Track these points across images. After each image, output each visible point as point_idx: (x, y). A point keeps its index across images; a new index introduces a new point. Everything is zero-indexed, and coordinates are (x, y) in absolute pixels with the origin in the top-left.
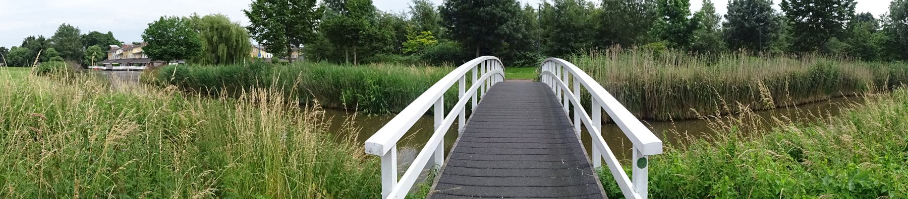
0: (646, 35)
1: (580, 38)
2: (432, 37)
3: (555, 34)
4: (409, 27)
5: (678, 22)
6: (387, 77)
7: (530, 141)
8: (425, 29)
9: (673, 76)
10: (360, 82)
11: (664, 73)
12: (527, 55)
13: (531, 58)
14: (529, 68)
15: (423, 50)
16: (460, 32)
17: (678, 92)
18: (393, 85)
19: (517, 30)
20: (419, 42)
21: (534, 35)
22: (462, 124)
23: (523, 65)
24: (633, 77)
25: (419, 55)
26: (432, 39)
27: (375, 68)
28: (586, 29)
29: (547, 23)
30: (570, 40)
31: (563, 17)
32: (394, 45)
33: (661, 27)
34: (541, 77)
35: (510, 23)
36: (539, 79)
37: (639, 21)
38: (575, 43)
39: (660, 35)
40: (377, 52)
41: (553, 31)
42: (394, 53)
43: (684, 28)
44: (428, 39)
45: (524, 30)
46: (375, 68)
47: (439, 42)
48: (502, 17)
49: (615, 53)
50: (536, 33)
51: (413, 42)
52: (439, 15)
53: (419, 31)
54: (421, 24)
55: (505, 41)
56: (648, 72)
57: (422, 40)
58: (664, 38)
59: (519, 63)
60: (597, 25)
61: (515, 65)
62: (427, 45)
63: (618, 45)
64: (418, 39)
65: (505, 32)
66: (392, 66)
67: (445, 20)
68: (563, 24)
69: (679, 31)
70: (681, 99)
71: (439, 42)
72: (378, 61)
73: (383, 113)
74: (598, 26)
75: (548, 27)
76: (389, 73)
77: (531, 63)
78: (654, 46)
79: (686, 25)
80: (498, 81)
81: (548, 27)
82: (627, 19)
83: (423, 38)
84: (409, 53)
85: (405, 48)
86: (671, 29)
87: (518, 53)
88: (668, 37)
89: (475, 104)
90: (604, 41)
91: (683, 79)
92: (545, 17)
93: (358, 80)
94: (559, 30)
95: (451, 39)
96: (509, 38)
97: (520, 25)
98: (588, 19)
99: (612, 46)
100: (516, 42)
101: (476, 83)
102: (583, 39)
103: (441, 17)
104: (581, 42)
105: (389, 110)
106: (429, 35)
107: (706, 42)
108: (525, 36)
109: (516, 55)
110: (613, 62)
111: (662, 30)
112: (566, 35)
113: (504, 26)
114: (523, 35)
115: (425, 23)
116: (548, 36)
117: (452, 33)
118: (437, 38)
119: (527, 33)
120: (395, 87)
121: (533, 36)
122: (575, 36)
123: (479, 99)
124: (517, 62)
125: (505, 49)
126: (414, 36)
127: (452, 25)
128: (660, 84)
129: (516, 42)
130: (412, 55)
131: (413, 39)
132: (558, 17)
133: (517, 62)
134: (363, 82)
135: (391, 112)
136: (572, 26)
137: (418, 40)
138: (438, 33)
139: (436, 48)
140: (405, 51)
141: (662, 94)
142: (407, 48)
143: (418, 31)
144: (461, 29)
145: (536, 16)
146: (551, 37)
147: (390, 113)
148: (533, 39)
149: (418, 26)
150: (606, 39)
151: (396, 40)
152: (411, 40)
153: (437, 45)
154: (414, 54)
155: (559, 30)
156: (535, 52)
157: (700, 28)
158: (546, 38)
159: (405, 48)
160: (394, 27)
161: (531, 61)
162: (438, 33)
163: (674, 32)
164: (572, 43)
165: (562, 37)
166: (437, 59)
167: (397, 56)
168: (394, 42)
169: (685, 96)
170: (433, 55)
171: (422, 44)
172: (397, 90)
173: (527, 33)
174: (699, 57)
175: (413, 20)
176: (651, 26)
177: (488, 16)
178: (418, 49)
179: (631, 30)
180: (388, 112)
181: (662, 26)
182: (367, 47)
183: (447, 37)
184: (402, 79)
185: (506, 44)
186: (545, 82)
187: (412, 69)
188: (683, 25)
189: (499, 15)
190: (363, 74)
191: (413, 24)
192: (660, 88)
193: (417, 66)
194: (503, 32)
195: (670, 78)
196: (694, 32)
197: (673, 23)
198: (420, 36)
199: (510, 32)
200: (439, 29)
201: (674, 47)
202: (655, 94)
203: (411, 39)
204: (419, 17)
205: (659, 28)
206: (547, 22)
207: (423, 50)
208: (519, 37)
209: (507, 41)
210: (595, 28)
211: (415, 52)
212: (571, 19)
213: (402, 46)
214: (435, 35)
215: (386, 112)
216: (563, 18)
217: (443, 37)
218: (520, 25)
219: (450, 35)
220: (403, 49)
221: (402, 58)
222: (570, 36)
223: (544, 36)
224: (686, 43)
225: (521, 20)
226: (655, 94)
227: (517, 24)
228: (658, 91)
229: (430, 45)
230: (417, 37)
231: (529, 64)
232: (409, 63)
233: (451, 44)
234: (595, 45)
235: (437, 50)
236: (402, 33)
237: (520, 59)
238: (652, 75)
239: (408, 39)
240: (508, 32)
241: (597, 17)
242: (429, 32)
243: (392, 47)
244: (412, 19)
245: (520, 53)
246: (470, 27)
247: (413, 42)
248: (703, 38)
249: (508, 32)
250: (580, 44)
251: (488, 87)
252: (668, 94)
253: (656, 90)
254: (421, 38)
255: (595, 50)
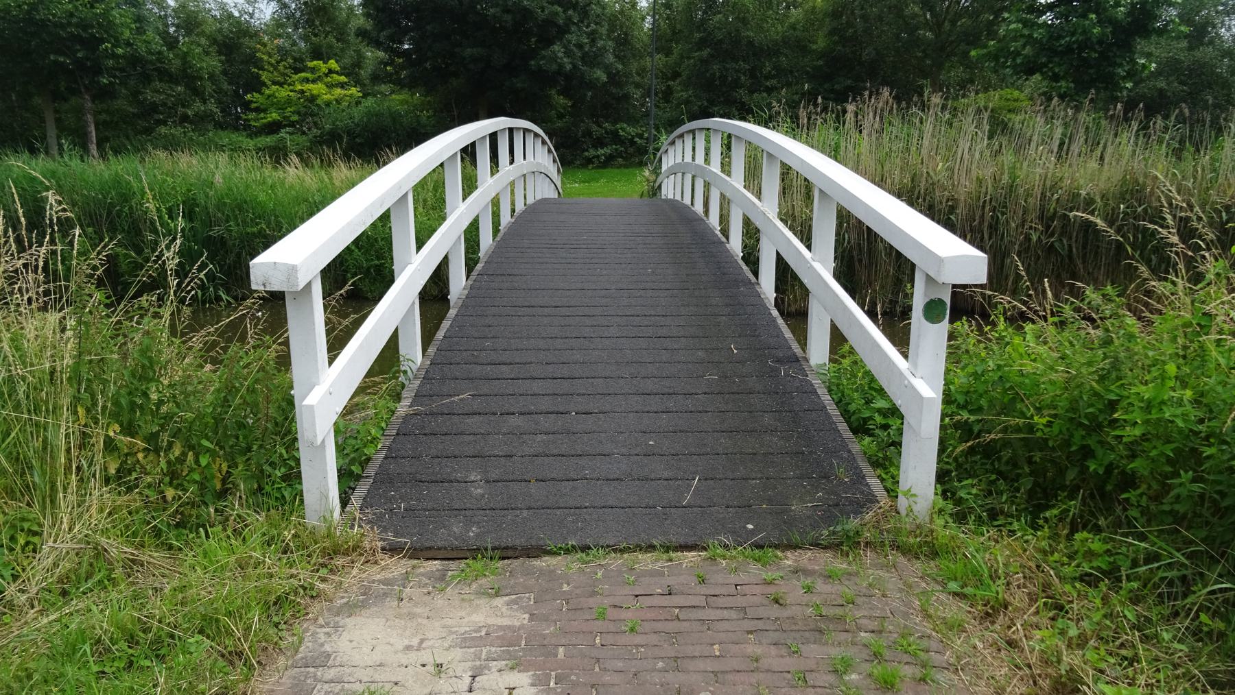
0: (969, 65)
1: (768, 77)
2: (343, 79)
3: (695, 65)
4: (265, 45)
5: (1084, 16)
6: (211, 193)
7: (639, 313)
8: (317, 54)
9: (1048, 183)
10: (121, 211)
11: (1021, 174)
12: (622, 133)
13: (632, 143)
14: (626, 171)
15: (316, 119)
16: (428, 65)
17: (1063, 234)
18: (236, 218)
19: (592, 59)
20: (302, 92)
21: (638, 74)
22: (413, 353)
23: (608, 162)
24: (923, 184)
25: (304, 133)
26: (342, 85)
27: (168, 166)
28: (785, 51)
29: (675, 35)
30: (736, 84)
31: (720, 13)
32: (219, 102)
33: (1022, 36)
34: (660, 187)
35: (573, 38)
36: (655, 191)
37: (953, 23)
38: (752, 92)
39: (1019, 61)
40: (164, 123)
41: (689, 58)
42: (220, 126)
43: (1104, 34)
44: (330, 86)
45: (611, 58)
46: (168, 166)
47: (365, 96)
48: (550, 22)
49: (871, 114)
50: (644, 69)
51: (283, 93)
52: (359, 11)
53: (301, 60)
54: (305, 38)
55: (560, 93)
56: (968, 171)
57: (311, 86)
58: (1029, 69)
59: (598, 157)
60: (819, 41)
61: (589, 161)
62: (328, 104)
63: (886, 92)
64: (300, 84)
65: (561, 66)
66: (223, 158)
67: (380, 25)
68: (719, 35)
69: (1085, 44)
70: (1070, 256)
71: (365, 96)
72: (171, 145)
73: (211, 302)
74: (821, 43)
75: (677, 49)
76: (218, 178)
77: (632, 155)
78: (995, 98)
79: (1112, 21)
80: (539, 197)
81: (677, 49)
82: (915, 16)
83: (314, 81)
84: (273, 128)
85: (257, 110)
86: (1060, 37)
87: (594, 128)
88: (1045, 65)
89: (458, 282)
90: (836, 87)
91: (1083, 193)
92: (668, 18)
93: (112, 205)
94: (705, 53)
95: (400, 84)
96: (572, 83)
97: (600, 43)
98: (792, 20)
99: (867, 93)
100: (590, 94)
101: (459, 213)
102: (774, 82)
103: (367, 15)
104: (769, 90)
105: (228, 293)
106: (331, 71)
107: (1181, 83)
108: (614, 78)
109: (588, 133)
110: (865, 142)
111: (1024, 46)
112: (727, 70)
113: (556, 47)
114: (610, 75)
115: (316, 35)
116: (676, 75)
117: (402, 67)
118: (358, 82)
119: (620, 67)
120: (244, 222)
121: (637, 79)
122: (752, 73)
123: (471, 264)
124: (592, 153)
125: (561, 116)
126: (284, 74)
127: (402, 43)
128: (1005, 207)
129: (590, 94)
130: (283, 133)
131: (281, 85)
132: (705, 12)
133: (592, 153)
134: (131, 208)
135: (236, 298)
136: (744, 42)
137: (299, 87)
138: (360, 68)
139: (357, 112)
140: (256, 120)
141: (1006, 240)
142: (265, 111)
143: (295, 59)
144: (429, 54)
145: (643, 19)
146: (685, 75)
147: (232, 301)
148: (638, 86)
149: (294, 44)
150: (842, 83)
151: (225, 86)
152: (274, 88)
153: (358, 103)
154: (288, 129)
155: (705, 53)
156: (641, 123)
157: (1162, 32)
158: (671, 83)
159: (257, 110)
160: (214, 41)
161: (631, 150)
162: (360, 68)
163: (1069, 50)
164: (742, 94)
165: (714, 74)
166: (360, 144)
167: (234, 136)
168: (219, 91)
169: (1084, 247)
170: (349, 133)
171: (313, 99)
172: (249, 230)
173: (620, 67)
174: (1146, 127)
175: (277, 24)
176: (992, 34)
177: (508, 17)
178: (299, 113)
179: (924, 51)
180: (224, 297)
181: (1026, 32)
182: (122, 104)
183: (388, 79)
184: (262, 197)
185: (562, 100)
186: (670, 196)
187: (291, 171)
188: (1100, 21)
189: (542, 16)
190: (128, 183)
191: (280, 36)
192: (1003, 219)
193: (306, 162)
194: (554, 67)
195: (1037, 192)
196: (1141, 44)
197: (1065, 16)
198: (303, 75)
199: (575, 66)
200: (360, 57)
201: (1062, 97)
202: (986, 236)
203: (274, 83)
204: (298, 14)
205: (1015, 39)
206: (674, 33)
207: (316, 119)
208: (597, 79)
209: (565, 92)
210: (814, 47)
211: (292, 124)
212: (744, 21)
213: (247, 106)
214: (352, 72)
215: (219, 299)
216: (720, 16)
217: (376, 78)
218: (600, 43)
219: (397, 73)
220: (252, 116)
221: (251, 144)
222: (737, 71)
223: (665, 77)
224: (1108, 83)
225: (605, 32)
226: (986, 236)
227: (593, 41)
228: (996, 230)
229: (338, 101)
230: (296, 77)
231: (625, 159)
232: (278, 155)
233: (402, 102)
234: (811, 97)
235: (361, 120)
236: (242, 62)
237: (599, 143)
238: (980, 181)
239: (264, 84)
240: (569, 67)
241: (820, 16)
242: (333, 64)
243: (213, 107)
244: (273, 19)
245: (600, 126)
246: (457, 50)
247: (283, 93)
248: (1171, 68)
249: (569, 67)
250: (765, 95)
251: (506, 219)
252: (1028, 238)
253: (990, 226)
254: (307, 80)
255: (816, 105)
